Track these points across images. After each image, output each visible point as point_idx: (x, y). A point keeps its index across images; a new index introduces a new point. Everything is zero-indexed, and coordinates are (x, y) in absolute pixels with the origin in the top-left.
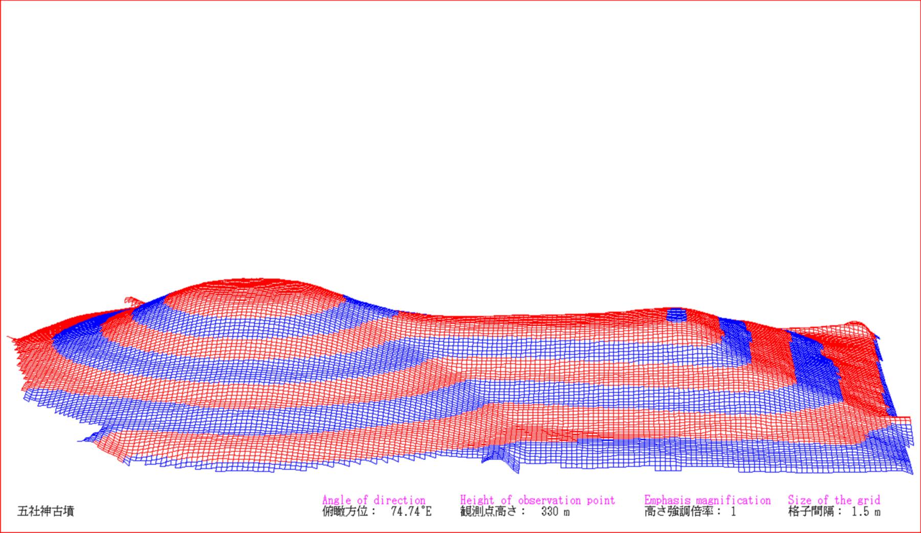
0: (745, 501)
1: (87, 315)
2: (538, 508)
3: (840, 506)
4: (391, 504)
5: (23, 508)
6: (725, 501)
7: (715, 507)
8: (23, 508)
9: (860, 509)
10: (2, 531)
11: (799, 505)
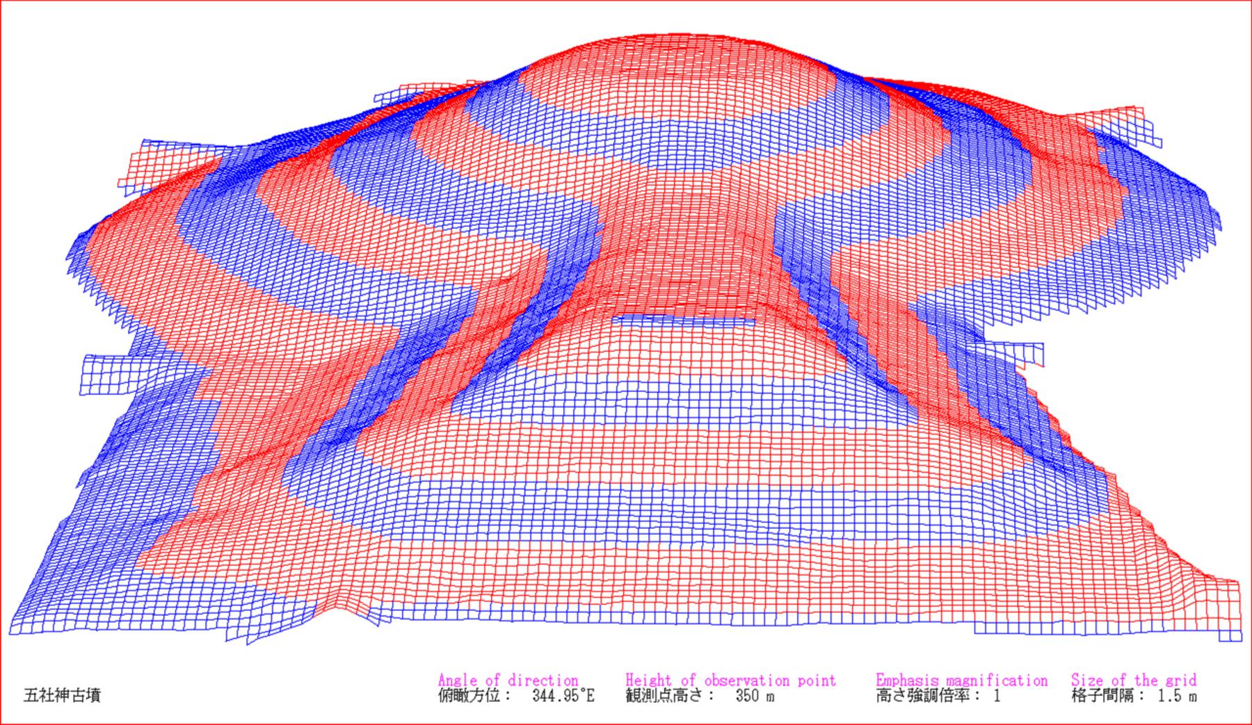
0: (1012, 682)
2: (731, 692)
3: (1142, 688)
5: (31, 692)
6: (986, 682)
7: (972, 690)
8: (31, 692)
9: (1169, 693)
10: (3, 722)
11: (1087, 687)
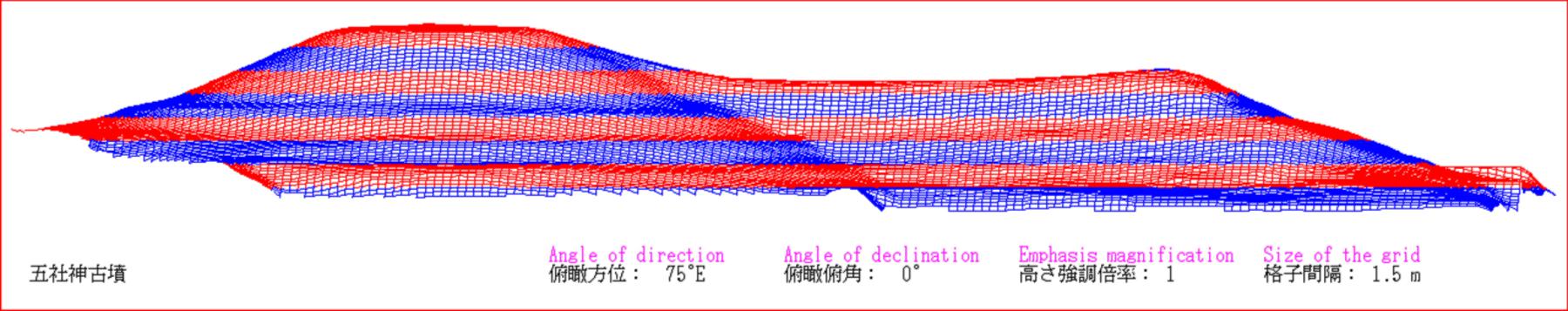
0: (1190, 257)
1: (1347, 133)
2: (895, 269)
3: (1352, 265)
4: (666, 262)
5: (38, 269)
6: (1156, 257)
7: (1139, 267)
8: (38, 269)
9: (1386, 271)
10: (4, 307)
11: (1283, 264)
